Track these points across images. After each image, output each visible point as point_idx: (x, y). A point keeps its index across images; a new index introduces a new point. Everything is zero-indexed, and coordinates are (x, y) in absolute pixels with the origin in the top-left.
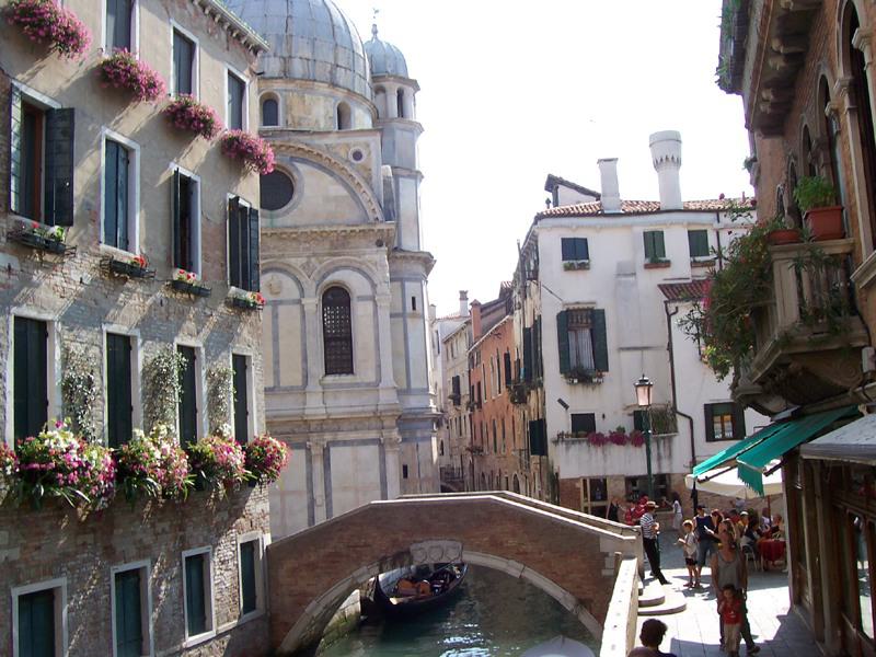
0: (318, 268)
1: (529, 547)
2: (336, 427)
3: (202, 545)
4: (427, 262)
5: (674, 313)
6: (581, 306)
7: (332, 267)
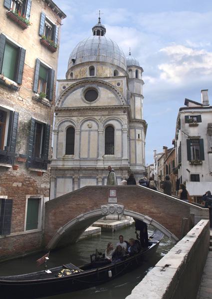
1: (154, 210)
7: (109, 119)
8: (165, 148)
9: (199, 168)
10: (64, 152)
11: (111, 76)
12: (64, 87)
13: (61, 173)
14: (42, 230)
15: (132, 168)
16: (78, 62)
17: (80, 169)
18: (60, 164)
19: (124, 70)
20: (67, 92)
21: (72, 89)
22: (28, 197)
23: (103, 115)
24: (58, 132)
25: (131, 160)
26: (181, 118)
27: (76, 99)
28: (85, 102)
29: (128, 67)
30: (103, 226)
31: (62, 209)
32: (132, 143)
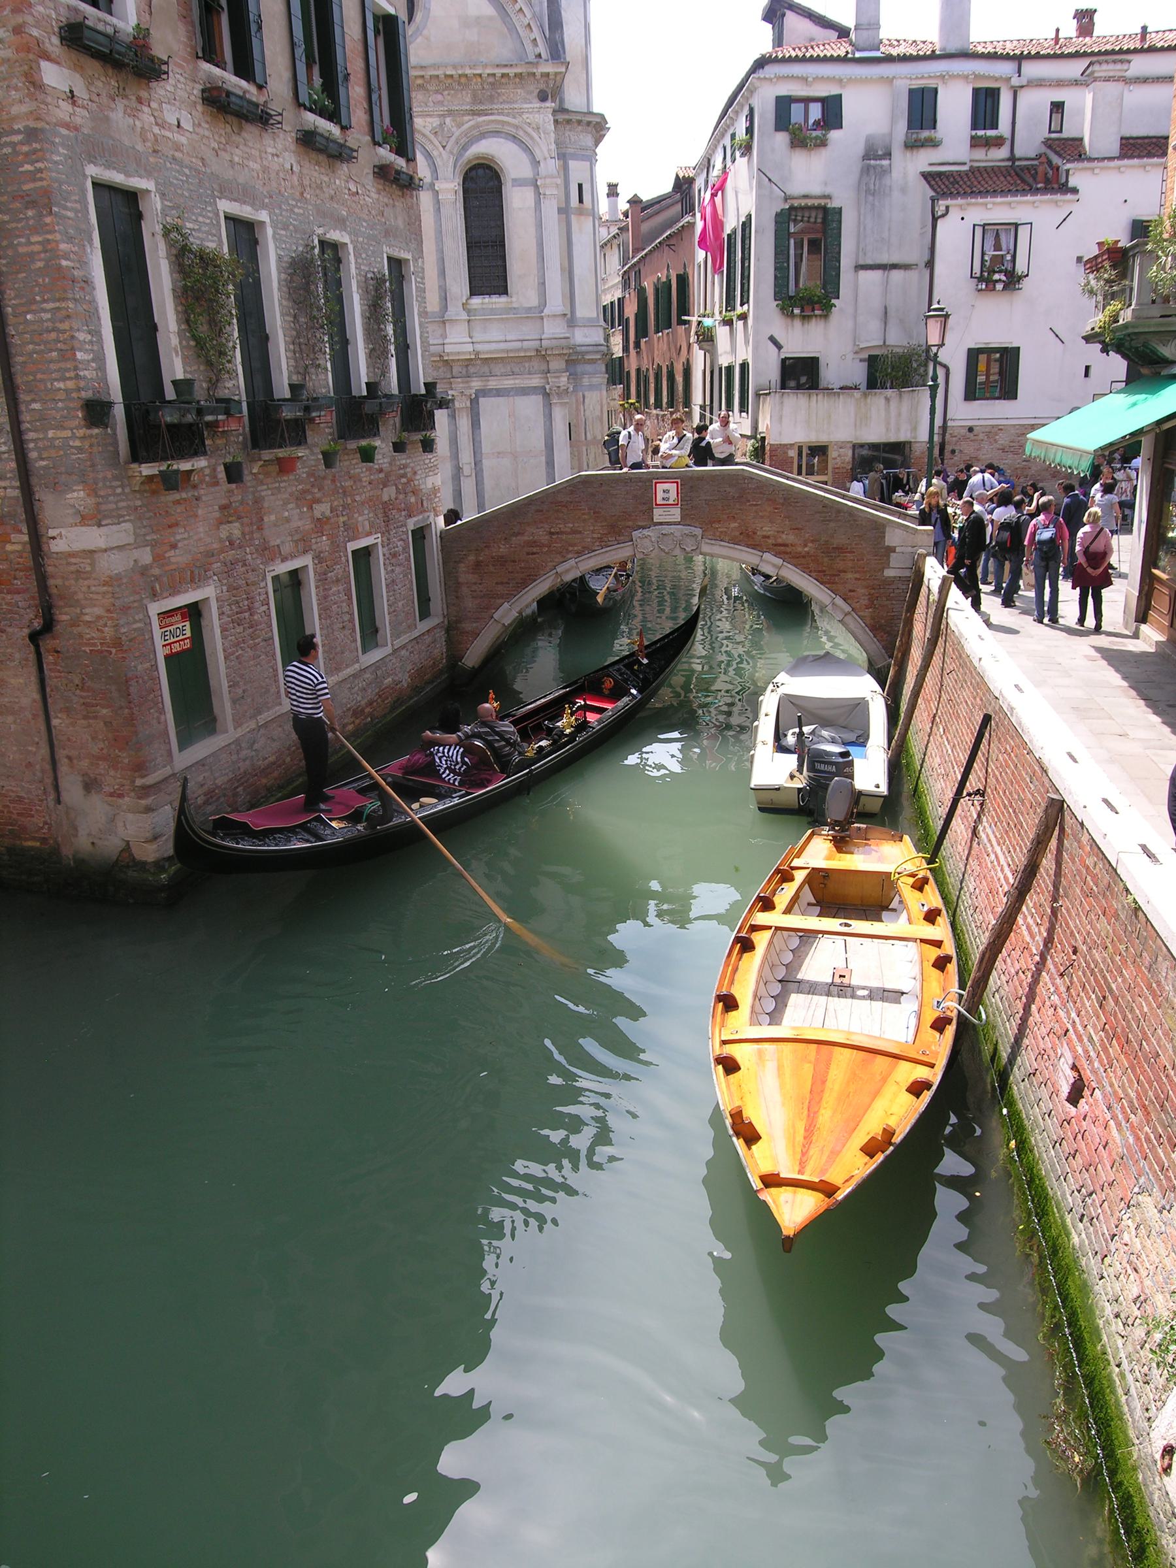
0: (457, 134)
1: (789, 538)
2: (486, 369)
3: (369, 534)
4: (598, 127)
5: (943, 216)
6: (810, 202)
7: (475, 132)
9: (816, 328)
31: (503, 549)
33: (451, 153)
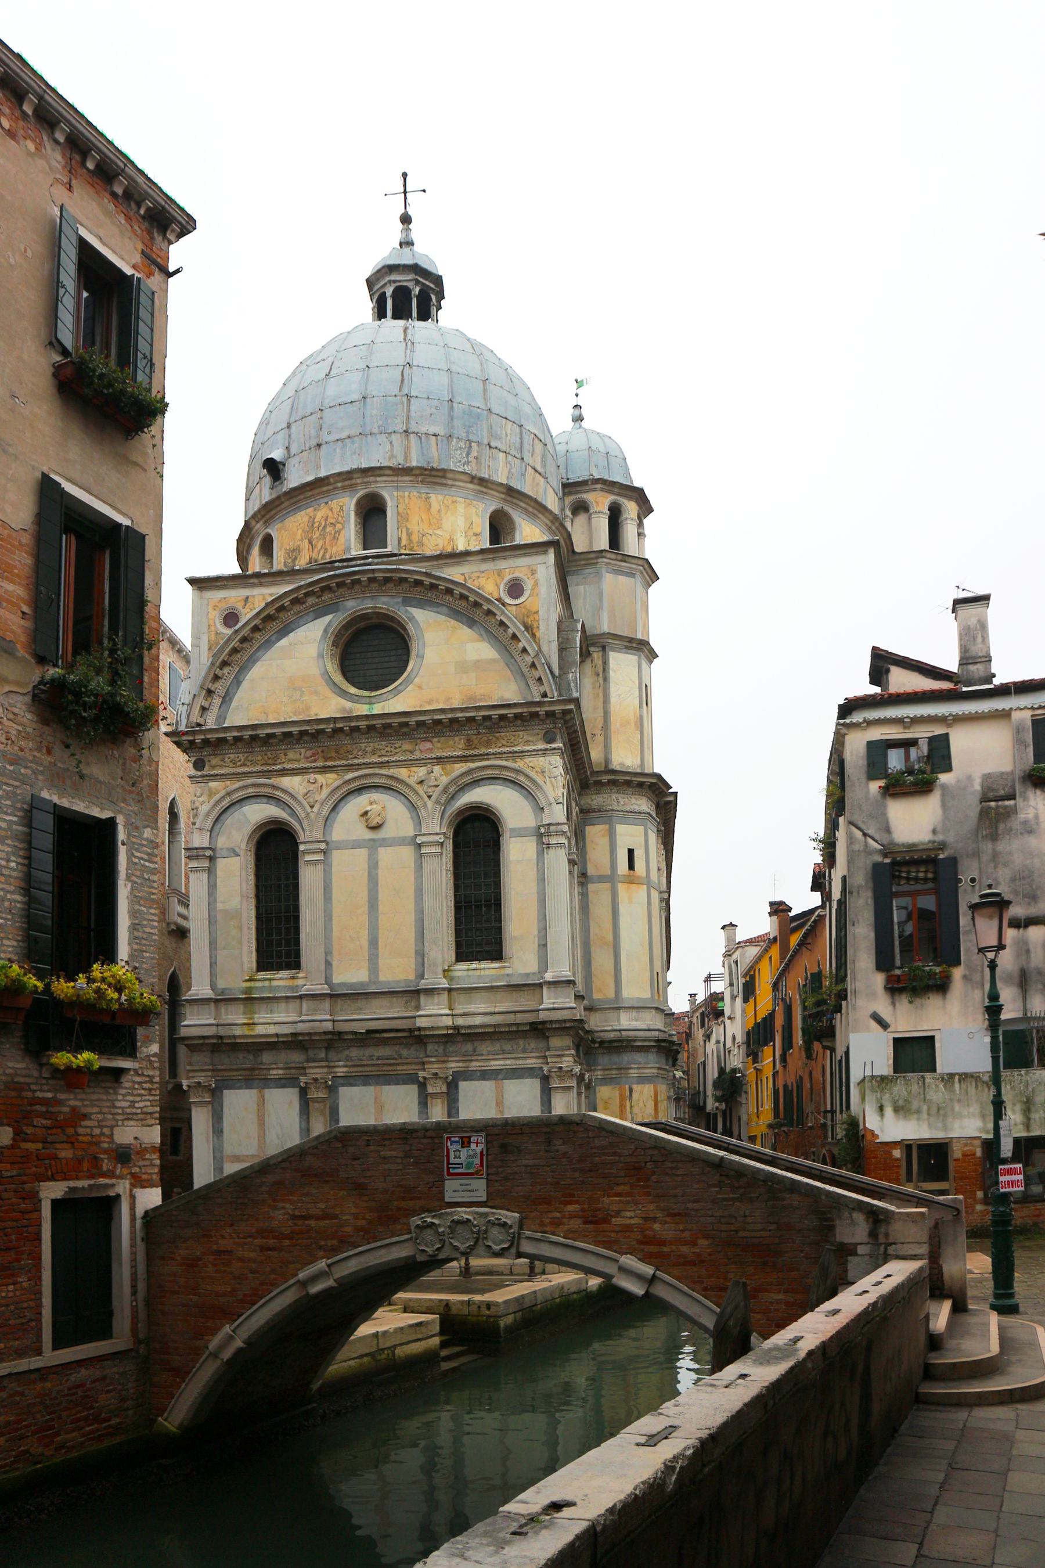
7: (467, 779)
8: (778, 909)
10: (249, 957)
11: (474, 547)
12: (230, 618)
13: (241, 1060)
14: (138, 1342)
15: (595, 1022)
16: (295, 477)
17: (335, 1040)
18: (235, 1021)
19: (543, 508)
20: (243, 644)
21: (275, 621)
22: (52, 1191)
23: (439, 760)
24: (212, 859)
25: (596, 983)
26: (848, 756)
27: (296, 677)
28: (343, 694)
29: (569, 487)
30: (454, 1310)
32: (599, 894)
33: (437, 802)
